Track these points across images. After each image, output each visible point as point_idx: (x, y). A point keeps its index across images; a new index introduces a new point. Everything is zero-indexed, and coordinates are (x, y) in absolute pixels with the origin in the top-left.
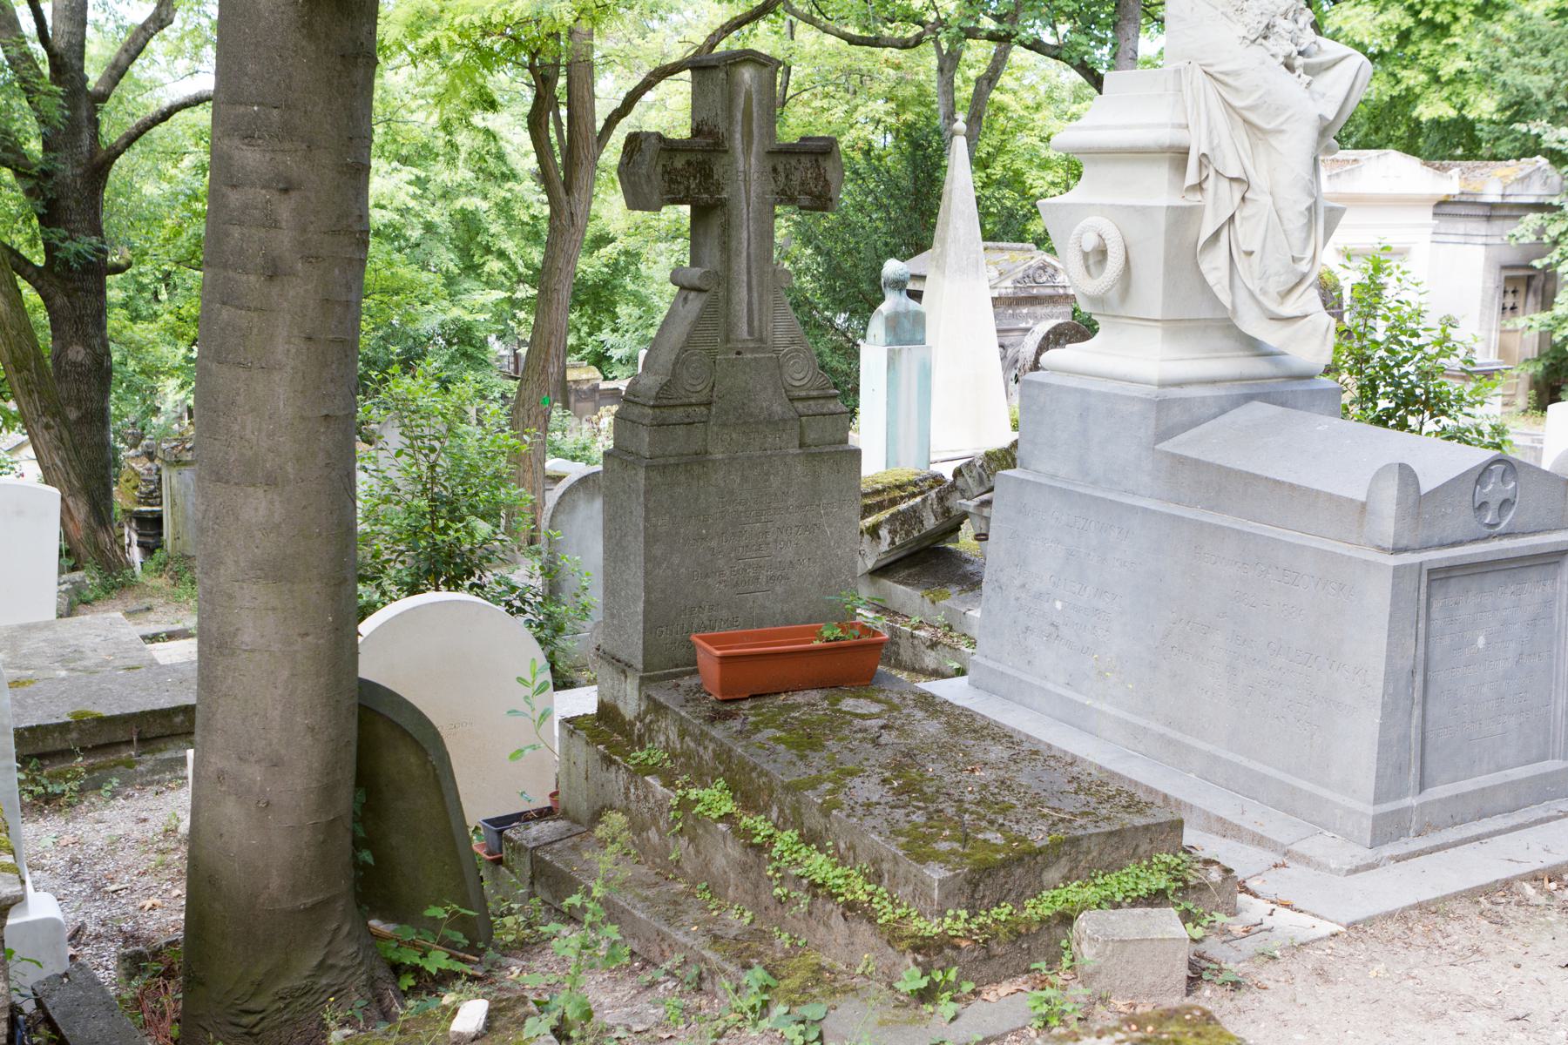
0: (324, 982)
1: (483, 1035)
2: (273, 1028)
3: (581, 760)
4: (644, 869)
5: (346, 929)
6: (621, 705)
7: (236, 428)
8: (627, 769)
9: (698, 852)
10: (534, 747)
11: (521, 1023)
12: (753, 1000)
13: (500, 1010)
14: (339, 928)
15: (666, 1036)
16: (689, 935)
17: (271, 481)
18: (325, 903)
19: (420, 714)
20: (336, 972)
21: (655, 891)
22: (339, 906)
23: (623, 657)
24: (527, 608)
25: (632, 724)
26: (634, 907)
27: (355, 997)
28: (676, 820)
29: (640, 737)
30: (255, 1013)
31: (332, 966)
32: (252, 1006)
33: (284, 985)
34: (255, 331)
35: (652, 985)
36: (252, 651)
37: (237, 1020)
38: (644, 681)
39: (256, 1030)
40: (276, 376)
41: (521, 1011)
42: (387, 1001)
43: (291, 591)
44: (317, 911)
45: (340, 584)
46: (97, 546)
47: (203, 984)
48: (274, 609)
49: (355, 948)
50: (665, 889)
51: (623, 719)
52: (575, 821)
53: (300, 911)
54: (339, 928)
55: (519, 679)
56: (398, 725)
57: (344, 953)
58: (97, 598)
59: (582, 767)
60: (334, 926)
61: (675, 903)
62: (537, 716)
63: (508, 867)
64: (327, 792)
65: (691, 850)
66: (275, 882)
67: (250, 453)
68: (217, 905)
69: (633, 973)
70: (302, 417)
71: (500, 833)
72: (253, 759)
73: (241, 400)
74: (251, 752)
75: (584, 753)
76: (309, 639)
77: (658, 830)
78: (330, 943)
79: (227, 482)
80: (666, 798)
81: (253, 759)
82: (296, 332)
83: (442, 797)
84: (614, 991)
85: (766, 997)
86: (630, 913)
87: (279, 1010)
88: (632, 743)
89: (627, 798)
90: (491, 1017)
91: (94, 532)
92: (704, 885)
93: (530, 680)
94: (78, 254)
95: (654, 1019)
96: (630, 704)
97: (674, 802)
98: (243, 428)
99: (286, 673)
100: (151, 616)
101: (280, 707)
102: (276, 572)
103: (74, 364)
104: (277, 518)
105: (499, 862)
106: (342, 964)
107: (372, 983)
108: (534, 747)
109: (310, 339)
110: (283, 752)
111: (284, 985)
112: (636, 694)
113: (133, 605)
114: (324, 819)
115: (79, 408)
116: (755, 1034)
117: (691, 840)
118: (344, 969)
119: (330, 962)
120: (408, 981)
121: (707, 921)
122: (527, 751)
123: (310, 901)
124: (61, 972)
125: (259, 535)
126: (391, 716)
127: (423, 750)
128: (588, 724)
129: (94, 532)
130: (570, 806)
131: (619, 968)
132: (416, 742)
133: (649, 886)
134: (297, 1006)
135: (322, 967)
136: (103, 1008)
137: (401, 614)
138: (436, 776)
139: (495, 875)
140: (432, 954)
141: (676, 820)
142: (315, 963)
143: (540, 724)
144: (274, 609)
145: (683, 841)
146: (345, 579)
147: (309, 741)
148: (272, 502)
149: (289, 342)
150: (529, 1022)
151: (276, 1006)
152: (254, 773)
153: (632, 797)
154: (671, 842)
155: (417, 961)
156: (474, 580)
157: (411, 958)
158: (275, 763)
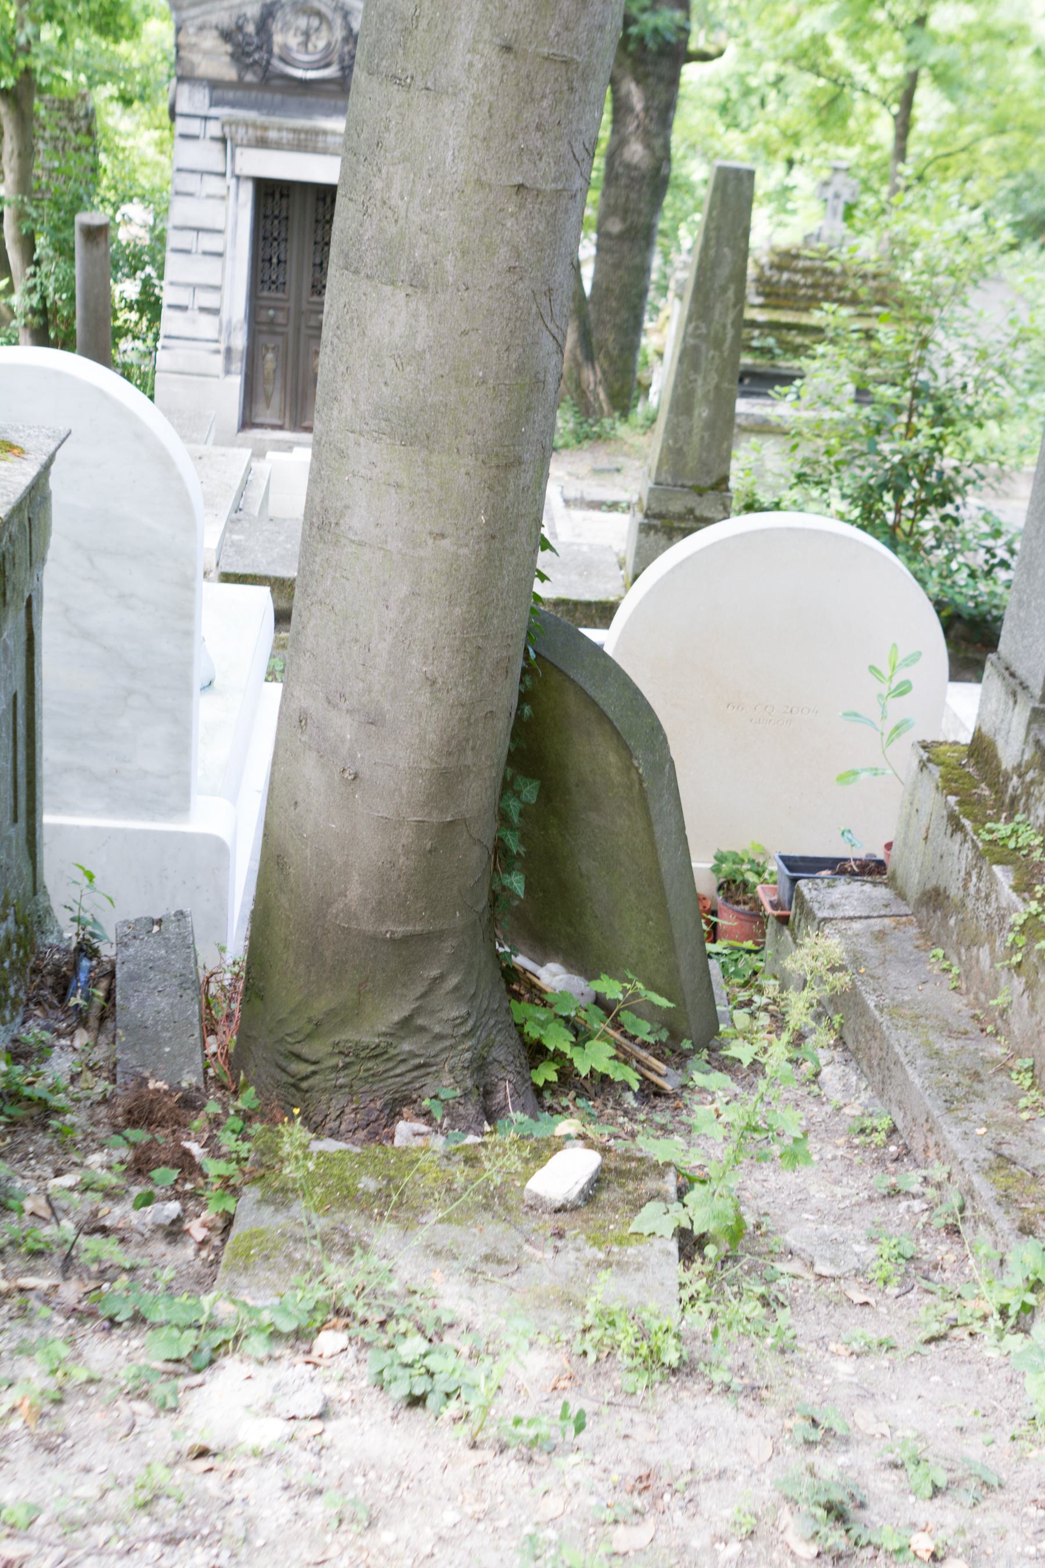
0: (406, 1047)
1: (576, 1208)
2: (325, 1090)
3: (926, 809)
4: (958, 1003)
5: (453, 981)
6: (1000, 743)
7: (378, 185)
8: (975, 846)
9: (1033, 1008)
10: (875, 772)
11: (637, 1206)
12: (1007, 1297)
13: (620, 1173)
14: (442, 978)
15: (859, 1297)
16: (966, 1141)
17: (418, 283)
18: (425, 938)
19: (637, 692)
20: (425, 1038)
21: (955, 1044)
22: (448, 946)
23: (1021, 671)
24: (1013, 562)
25: (1008, 779)
26: (912, 1063)
27: (448, 1080)
28: (1013, 948)
29: (1014, 800)
30: (306, 1061)
31: (422, 1029)
32: (305, 1050)
33: (349, 1036)
34: (423, 24)
35: (894, 1193)
36: (361, 544)
37: (284, 1063)
38: (1036, 714)
39: (304, 1085)
40: (446, 107)
41: (651, 1184)
42: (500, 1097)
43: (427, 464)
44: (410, 949)
45: (508, 466)
46: (578, 384)
47: (262, 998)
48: (398, 486)
49: (463, 1011)
50: (972, 1046)
51: (998, 766)
52: (901, 895)
53: (385, 940)
54: (442, 978)
55: (872, 668)
56: (595, 704)
57: (444, 1015)
58: (566, 446)
59: (924, 821)
60: (435, 973)
61: (976, 1076)
62: (889, 726)
63: (792, 931)
64: (446, 781)
65: (1026, 1001)
66: (355, 891)
67: (392, 230)
68: (284, 900)
69: (880, 1161)
70: (478, 181)
71: (794, 880)
72: (344, 706)
73: (390, 139)
74: (342, 696)
75: (934, 803)
76: (446, 543)
77: (992, 951)
78: (424, 995)
79: (356, 272)
80: (1012, 909)
81: (344, 706)
82: (486, 34)
83: (650, 824)
84: (837, 1182)
85: (1031, 1299)
86: (904, 1071)
87: (335, 1068)
88: (999, 805)
89: (965, 887)
90: (598, 1182)
91: (578, 366)
92: (1029, 1062)
93: (887, 671)
94: (656, 31)
95: (854, 1262)
96: (1012, 750)
97: (1018, 918)
98: (388, 186)
99: (404, 590)
100: (618, 478)
101: (389, 638)
102: (412, 429)
103: (628, 166)
104: (420, 344)
105: (784, 920)
106: (437, 1029)
107: (480, 1066)
108: (875, 772)
109: (507, 49)
110: (387, 706)
111: (349, 1036)
112: (1022, 732)
113: (604, 462)
114: (435, 818)
115: (624, 220)
116: (993, 1354)
117: (1029, 987)
118: (439, 1037)
119: (420, 1021)
120: (547, 1073)
121: (1006, 1124)
122: (864, 775)
123: (401, 930)
124: (156, 917)
125: (390, 364)
126: (587, 687)
127: (626, 747)
128: (951, 756)
129: (578, 366)
130: (900, 872)
131: (865, 1147)
132: (618, 734)
133: (953, 1033)
134: (359, 1070)
135: (407, 1026)
136: (176, 982)
137: (741, 536)
138: (642, 791)
139: (778, 932)
140: (593, 1045)
141: (1013, 948)
142: (396, 1018)
143: (890, 741)
144: (398, 486)
145: (1019, 983)
146: (519, 461)
147: (424, 698)
148: (415, 316)
149: (473, 50)
150: (651, 1208)
151: (333, 1062)
152: (344, 727)
153: (972, 890)
154: (1004, 975)
155: (566, 1048)
156: (949, 509)
157: (558, 1040)
158: (373, 721)
